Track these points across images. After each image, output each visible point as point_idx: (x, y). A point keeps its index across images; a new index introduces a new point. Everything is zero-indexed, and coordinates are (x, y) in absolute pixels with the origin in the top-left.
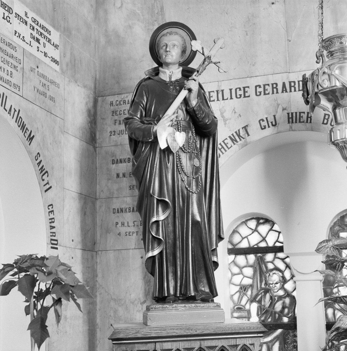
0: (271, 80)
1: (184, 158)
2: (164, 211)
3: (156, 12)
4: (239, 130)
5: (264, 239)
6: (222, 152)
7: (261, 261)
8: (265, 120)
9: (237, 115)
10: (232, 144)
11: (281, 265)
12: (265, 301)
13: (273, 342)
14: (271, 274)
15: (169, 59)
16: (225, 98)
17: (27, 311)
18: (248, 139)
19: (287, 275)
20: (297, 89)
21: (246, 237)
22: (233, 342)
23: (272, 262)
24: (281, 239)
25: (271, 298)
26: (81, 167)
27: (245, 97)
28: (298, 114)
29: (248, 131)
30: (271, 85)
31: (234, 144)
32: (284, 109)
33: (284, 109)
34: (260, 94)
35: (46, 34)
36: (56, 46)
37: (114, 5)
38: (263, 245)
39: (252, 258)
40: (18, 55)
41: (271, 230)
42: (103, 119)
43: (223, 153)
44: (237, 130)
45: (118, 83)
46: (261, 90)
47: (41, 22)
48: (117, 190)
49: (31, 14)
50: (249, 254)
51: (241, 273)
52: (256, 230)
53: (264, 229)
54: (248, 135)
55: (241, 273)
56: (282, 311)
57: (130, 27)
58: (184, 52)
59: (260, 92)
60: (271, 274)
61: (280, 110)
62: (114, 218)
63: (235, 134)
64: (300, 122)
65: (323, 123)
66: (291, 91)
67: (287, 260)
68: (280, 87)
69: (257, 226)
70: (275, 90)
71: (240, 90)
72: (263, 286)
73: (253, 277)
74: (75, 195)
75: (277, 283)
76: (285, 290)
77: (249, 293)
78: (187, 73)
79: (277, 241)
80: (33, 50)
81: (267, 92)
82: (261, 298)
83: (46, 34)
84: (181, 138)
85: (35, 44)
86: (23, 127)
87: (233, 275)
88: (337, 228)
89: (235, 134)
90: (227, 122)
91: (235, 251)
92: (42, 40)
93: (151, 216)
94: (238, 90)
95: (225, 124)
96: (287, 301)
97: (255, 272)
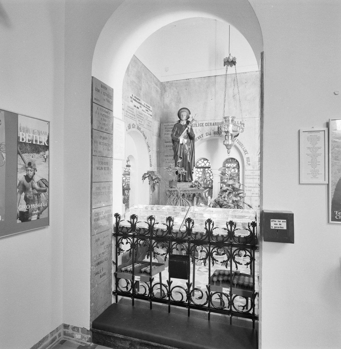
1: (186, 146)
2: (181, 159)
5: (205, 165)
7: (204, 170)
9: (200, 131)
11: (210, 172)
13: (206, 192)
15: (183, 119)
17: (150, 184)
18: (203, 138)
19: (211, 174)
22: (197, 192)
23: (207, 171)
24: (210, 165)
26: (157, 144)
32: (213, 130)
33: (213, 130)
35: (149, 108)
36: (151, 111)
38: (205, 166)
39: (202, 169)
41: (207, 162)
42: (163, 130)
45: (167, 120)
46: (207, 124)
47: (148, 105)
48: (166, 150)
50: (201, 168)
51: (199, 173)
52: (203, 162)
53: (205, 162)
55: (199, 173)
56: (209, 184)
58: (187, 117)
61: (212, 131)
62: (165, 158)
67: (211, 171)
68: (212, 124)
73: (202, 175)
74: (155, 152)
76: (210, 178)
77: (201, 179)
78: (188, 122)
79: (209, 165)
80: (146, 114)
83: (149, 108)
84: (186, 141)
85: (147, 112)
86: (144, 136)
87: (197, 174)
91: (198, 167)
92: (148, 110)
93: (177, 160)
96: (211, 181)
97: (202, 173)
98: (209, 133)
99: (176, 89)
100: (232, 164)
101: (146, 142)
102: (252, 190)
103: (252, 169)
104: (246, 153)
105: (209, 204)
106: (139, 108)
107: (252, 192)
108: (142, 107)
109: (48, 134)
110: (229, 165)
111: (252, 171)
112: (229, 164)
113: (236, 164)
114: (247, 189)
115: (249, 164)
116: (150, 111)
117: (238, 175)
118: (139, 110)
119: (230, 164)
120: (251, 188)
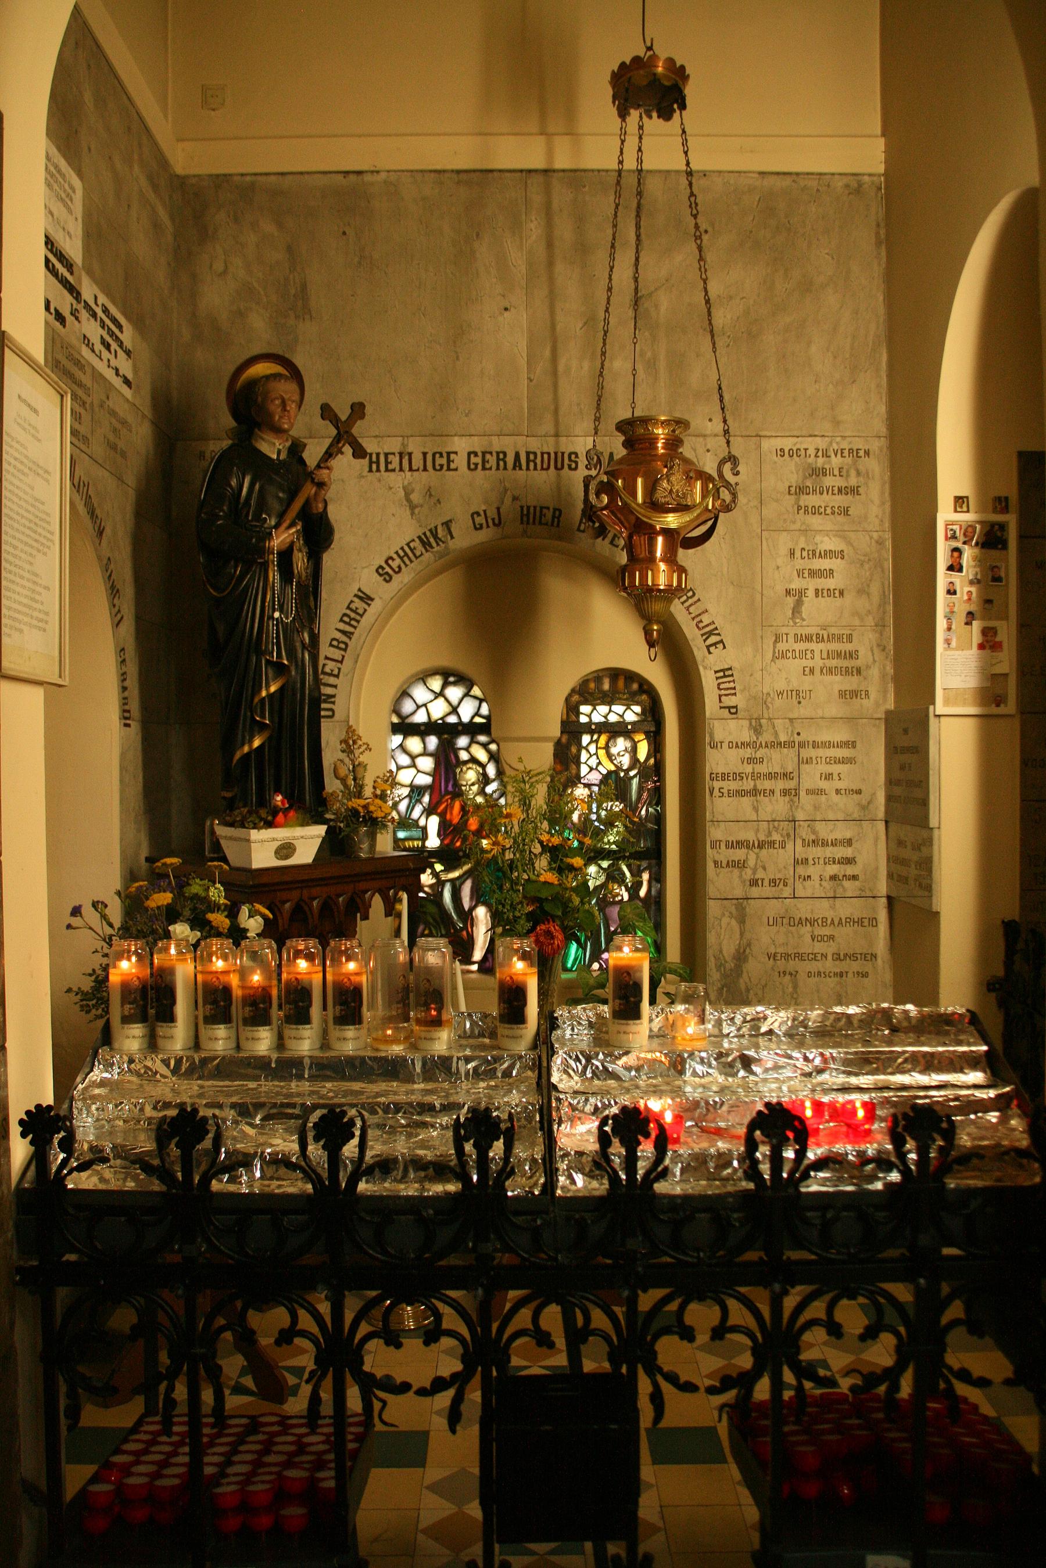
0: (497, 444)
3: (293, 292)
4: (436, 527)
5: (454, 710)
6: (404, 562)
8: (482, 513)
9: (433, 500)
10: (424, 551)
12: (451, 814)
13: (462, 879)
14: (464, 769)
16: (414, 467)
20: (539, 467)
21: (425, 705)
23: (467, 749)
25: (463, 808)
27: (449, 469)
28: (538, 509)
29: (452, 529)
30: (495, 454)
31: (427, 551)
32: (515, 498)
33: (515, 498)
34: (476, 468)
37: (211, 266)
39: (433, 742)
40: (86, 380)
41: (467, 695)
43: (406, 565)
44: (432, 526)
46: (479, 460)
49: (102, 299)
51: (414, 765)
52: (441, 694)
53: (454, 693)
54: (452, 537)
55: (414, 765)
57: (241, 314)
59: (476, 465)
60: (464, 769)
63: (428, 534)
64: (540, 523)
65: (579, 530)
66: (528, 469)
68: (510, 459)
69: (444, 687)
70: (501, 463)
71: (441, 455)
72: (450, 788)
73: (435, 774)
75: (473, 784)
77: (426, 799)
80: (101, 367)
81: (488, 466)
82: (446, 807)
85: (105, 354)
88: (576, 698)
89: (428, 534)
90: (416, 511)
94: (437, 456)
95: (412, 514)
98: (492, 513)
99: (280, 225)
100: (619, 709)
101: (100, 558)
102: (751, 863)
103: (746, 736)
104: (715, 644)
105: (478, 955)
106: (69, 319)
107: (748, 874)
108: (84, 315)
109: (720, 344)
110: (599, 714)
111: (748, 752)
112: (614, 708)
113: (637, 709)
114: (725, 854)
115: (733, 710)
116: (121, 354)
117: (655, 770)
118: (63, 330)
119: (603, 709)
120: (744, 851)
